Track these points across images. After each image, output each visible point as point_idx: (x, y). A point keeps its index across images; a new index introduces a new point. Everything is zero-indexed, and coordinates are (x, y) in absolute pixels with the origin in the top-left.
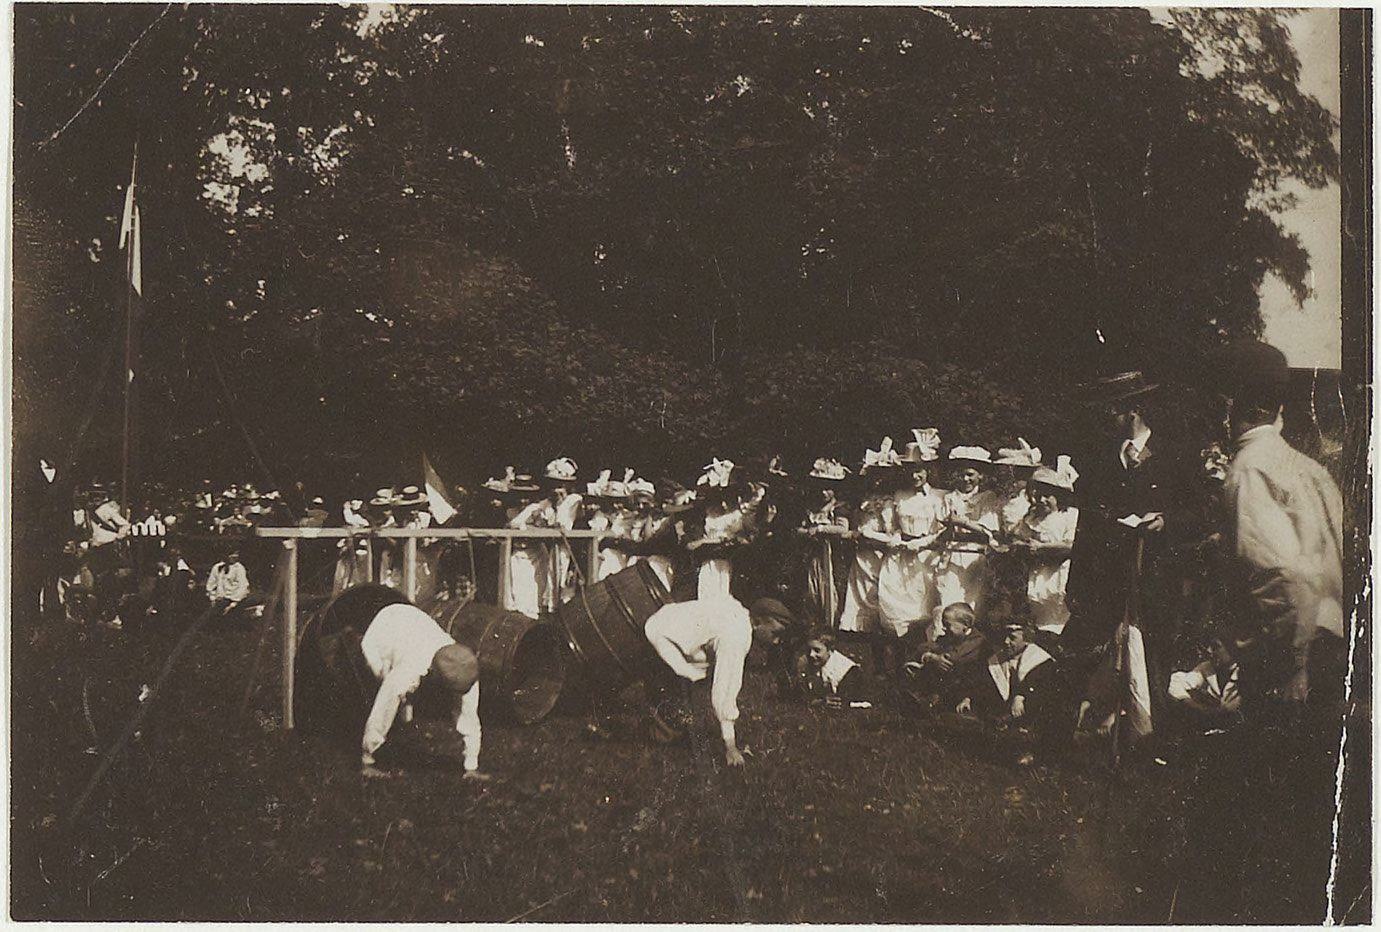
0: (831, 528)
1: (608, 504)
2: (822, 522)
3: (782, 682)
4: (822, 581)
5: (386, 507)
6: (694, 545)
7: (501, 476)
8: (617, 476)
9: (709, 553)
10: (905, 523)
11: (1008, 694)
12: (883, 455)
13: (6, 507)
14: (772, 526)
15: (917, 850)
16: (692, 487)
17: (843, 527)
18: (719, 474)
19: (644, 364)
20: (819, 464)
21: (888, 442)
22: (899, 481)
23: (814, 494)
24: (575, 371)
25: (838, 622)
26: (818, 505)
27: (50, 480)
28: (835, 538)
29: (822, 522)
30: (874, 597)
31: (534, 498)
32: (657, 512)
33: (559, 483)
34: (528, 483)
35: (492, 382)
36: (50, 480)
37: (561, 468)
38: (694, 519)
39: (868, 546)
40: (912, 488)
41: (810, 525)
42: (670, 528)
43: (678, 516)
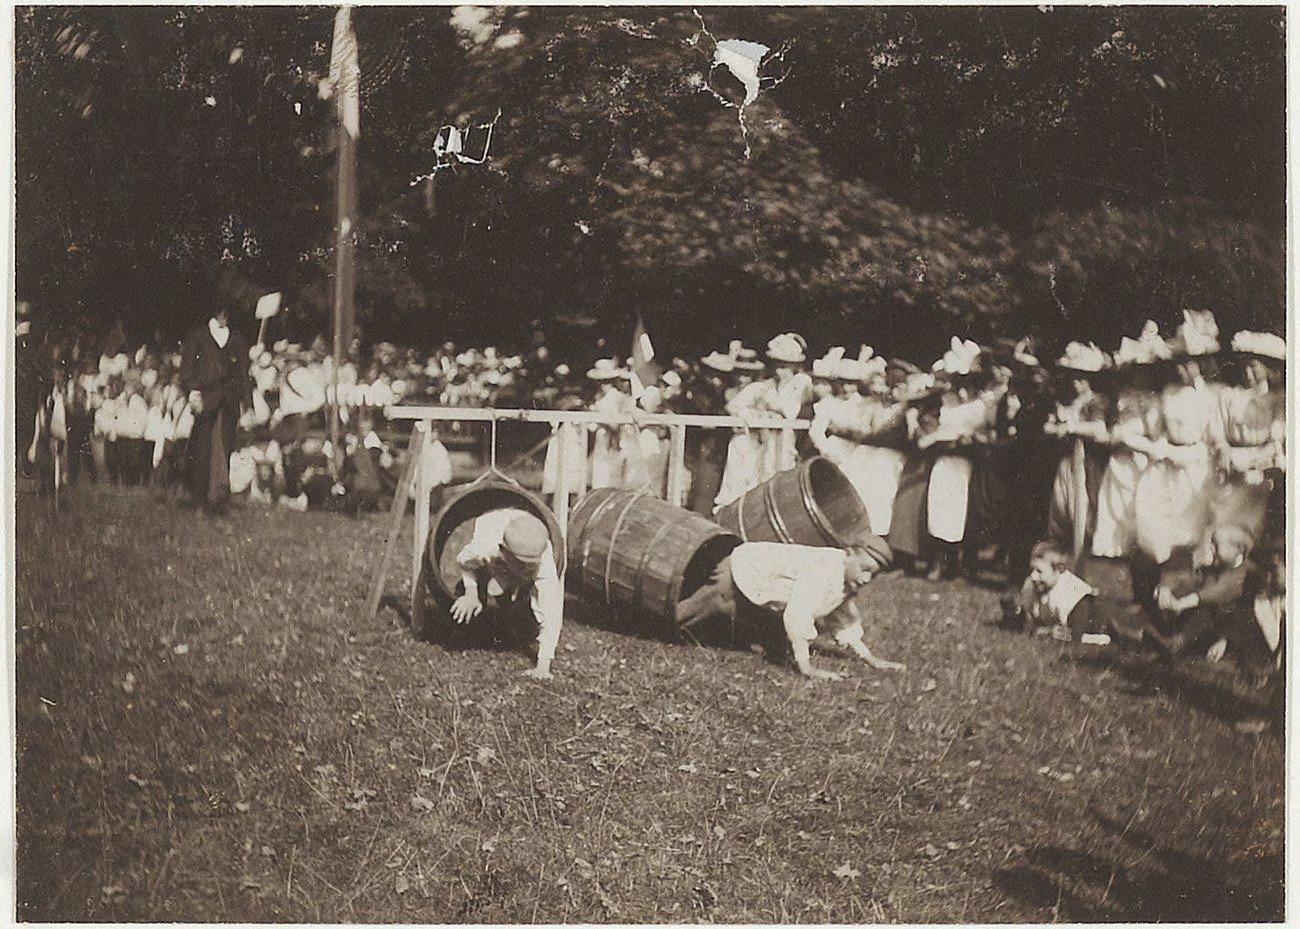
0: (1085, 428)
1: (837, 385)
2: (1069, 420)
3: (1007, 605)
4: (1070, 487)
5: (1072, 437)
6: (925, 442)
7: (724, 350)
8: (852, 354)
9: (941, 449)
10: (1173, 427)
11: (1277, 644)
12: (1145, 347)
13: (8, 554)
14: (1015, 422)
15: (1141, 812)
16: (926, 369)
17: (1098, 430)
18: (962, 356)
19: (917, 225)
20: (1073, 348)
21: (1152, 327)
22: (1160, 377)
23: (1063, 386)
24: (833, 231)
25: (1089, 541)
26: (1069, 396)
27: (222, 344)
28: (1089, 442)
29: (1069, 420)
30: (1131, 514)
31: (755, 376)
32: (887, 400)
33: (783, 364)
34: (752, 360)
35: (738, 241)
36: (222, 344)
37: (786, 347)
38: (930, 405)
39: (1122, 450)
40: (1178, 381)
41: (1058, 422)
42: (902, 421)
43: (912, 404)
